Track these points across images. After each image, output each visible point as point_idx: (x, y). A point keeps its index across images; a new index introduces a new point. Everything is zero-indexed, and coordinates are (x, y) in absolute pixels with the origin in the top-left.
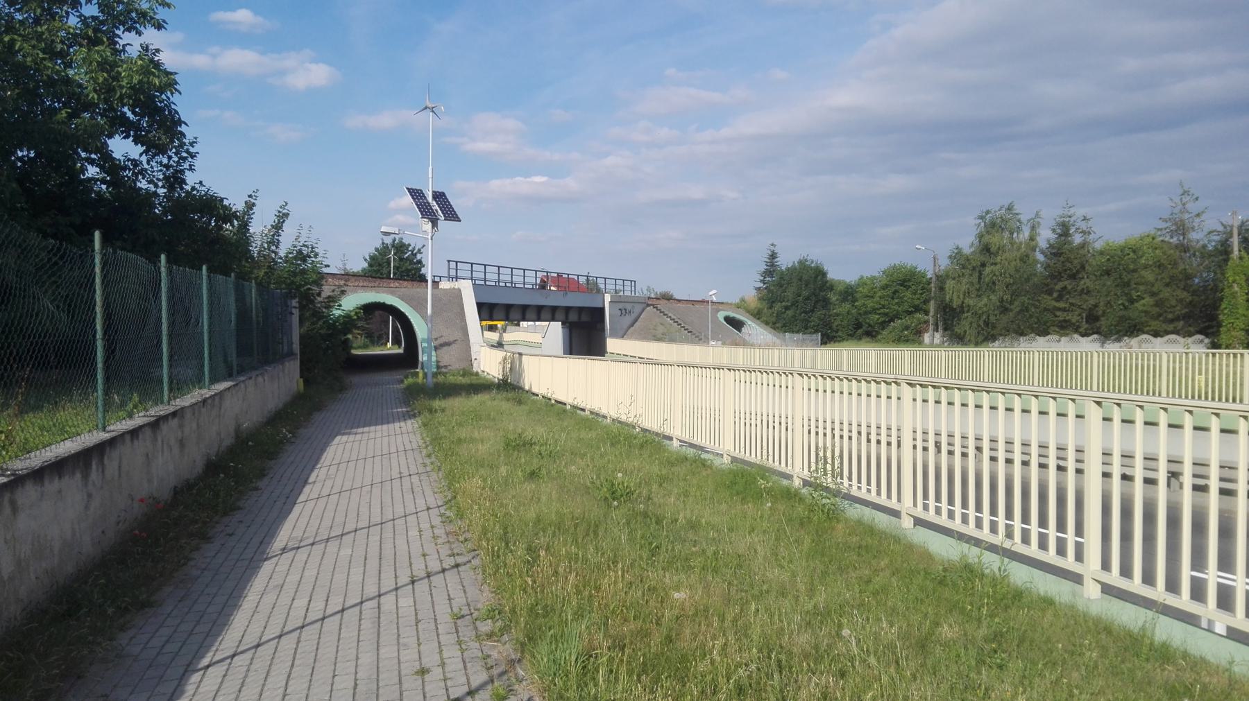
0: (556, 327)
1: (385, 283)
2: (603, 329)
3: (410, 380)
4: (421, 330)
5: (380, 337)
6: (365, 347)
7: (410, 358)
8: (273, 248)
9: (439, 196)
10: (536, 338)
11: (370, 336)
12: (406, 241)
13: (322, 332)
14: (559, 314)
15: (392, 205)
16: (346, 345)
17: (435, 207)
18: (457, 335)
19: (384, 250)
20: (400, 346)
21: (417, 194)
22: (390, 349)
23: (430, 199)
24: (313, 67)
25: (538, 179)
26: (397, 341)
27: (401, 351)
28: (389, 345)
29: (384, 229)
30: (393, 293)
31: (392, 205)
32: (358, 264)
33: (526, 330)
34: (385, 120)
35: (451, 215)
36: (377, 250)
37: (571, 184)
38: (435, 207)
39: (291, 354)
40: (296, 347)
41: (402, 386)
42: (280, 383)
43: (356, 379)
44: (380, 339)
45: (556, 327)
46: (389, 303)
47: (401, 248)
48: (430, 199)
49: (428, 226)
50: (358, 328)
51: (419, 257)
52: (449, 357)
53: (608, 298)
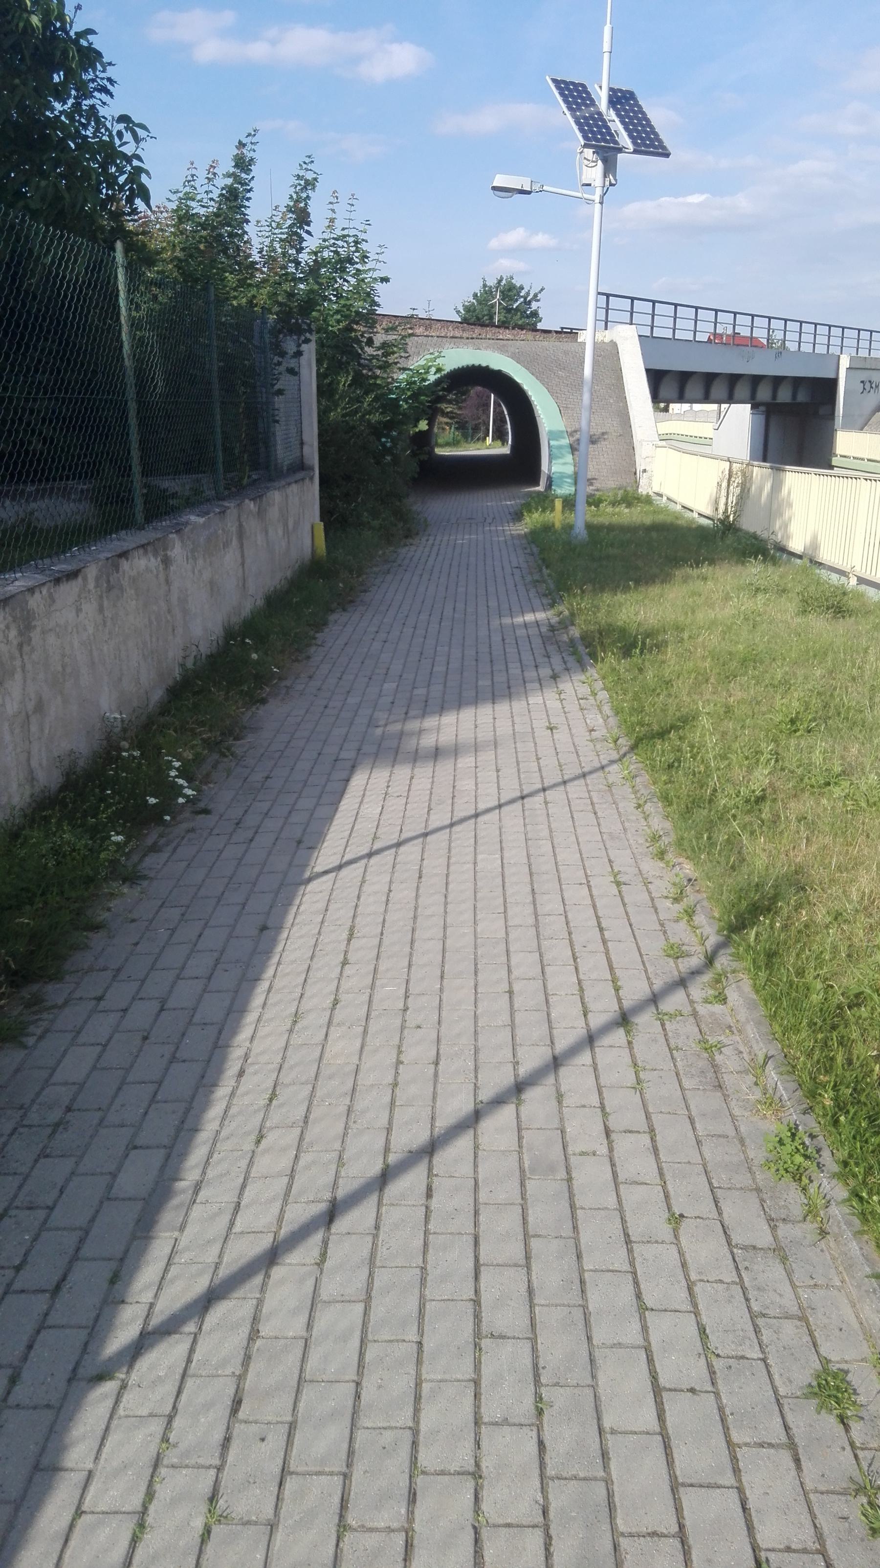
0: (740, 417)
1: (490, 332)
2: (831, 415)
3: (533, 519)
4: (548, 416)
5: (476, 429)
6: (455, 443)
7: (524, 463)
8: (292, 252)
9: (621, 99)
10: (705, 429)
11: (462, 426)
12: (517, 282)
13: (375, 418)
14: (742, 390)
15: (494, 243)
16: (424, 440)
17: (616, 126)
18: (611, 425)
19: (488, 292)
20: (504, 441)
21: (575, 95)
22: (491, 447)
23: (603, 104)
24: (395, 48)
25: (696, 199)
26: (500, 435)
27: (506, 450)
28: (489, 440)
29: (500, 180)
30: (502, 350)
31: (494, 243)
32: (449, 309)
33: (681, 417)
34: (487, 120)
35: (649, 143)
36: (475, 295)
37: (743, 203)
38: (616, 126)
39: (300, 467)
40: (312, 454)
41: (522, 528)
42: (288, 522)
43: (439, 507)
44: (471, 430)
45: (740, 417)
46: (495, 366)
47: (510, 291)
48: (603, 104)
49: (594, 173)
50: (444, 414)
51: (534, 306)
52: (604, 477)
53: (845, 362)
